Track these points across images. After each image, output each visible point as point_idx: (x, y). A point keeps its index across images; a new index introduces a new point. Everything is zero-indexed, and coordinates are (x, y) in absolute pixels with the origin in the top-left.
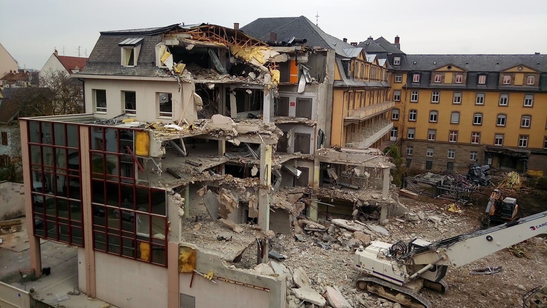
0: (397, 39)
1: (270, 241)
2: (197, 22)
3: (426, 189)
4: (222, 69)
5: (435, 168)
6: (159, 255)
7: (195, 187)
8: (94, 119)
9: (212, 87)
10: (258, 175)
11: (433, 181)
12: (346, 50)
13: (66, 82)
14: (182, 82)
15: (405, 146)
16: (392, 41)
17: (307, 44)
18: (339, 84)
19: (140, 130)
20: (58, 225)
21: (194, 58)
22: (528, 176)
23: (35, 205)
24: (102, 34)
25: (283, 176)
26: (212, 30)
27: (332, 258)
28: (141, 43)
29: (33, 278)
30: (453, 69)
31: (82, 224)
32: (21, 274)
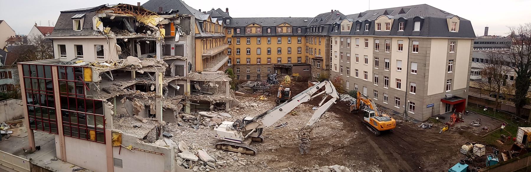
0: (227, 9)
1: (163, 127)
2: (116, 3)
3: (248, 90)
4: (132, 30)
5: (252, 78)
6: (100, 137)
7: (119, 98)
8: (60, 62)
9: (126, 40)
10: (155, 90)
11: (251, 85)
12: (201, 16)
13: (42, 41)
14: (109, 38)
15: (235, 68)
16: (225, 11)
17: (179, 13)
18: (198, 36)
19: (86, 67)
20: (43, 122)
21: (115, 24)
22: (293, 77)
23: (29, 111)
24: (62, 12)
25: (169, 89)
26: (125, 7)
27: (200, 134)
28: (84, 16)
29: (31, 152)
30: (256, 25)
31: (56, 121)
32: (24, 150)
